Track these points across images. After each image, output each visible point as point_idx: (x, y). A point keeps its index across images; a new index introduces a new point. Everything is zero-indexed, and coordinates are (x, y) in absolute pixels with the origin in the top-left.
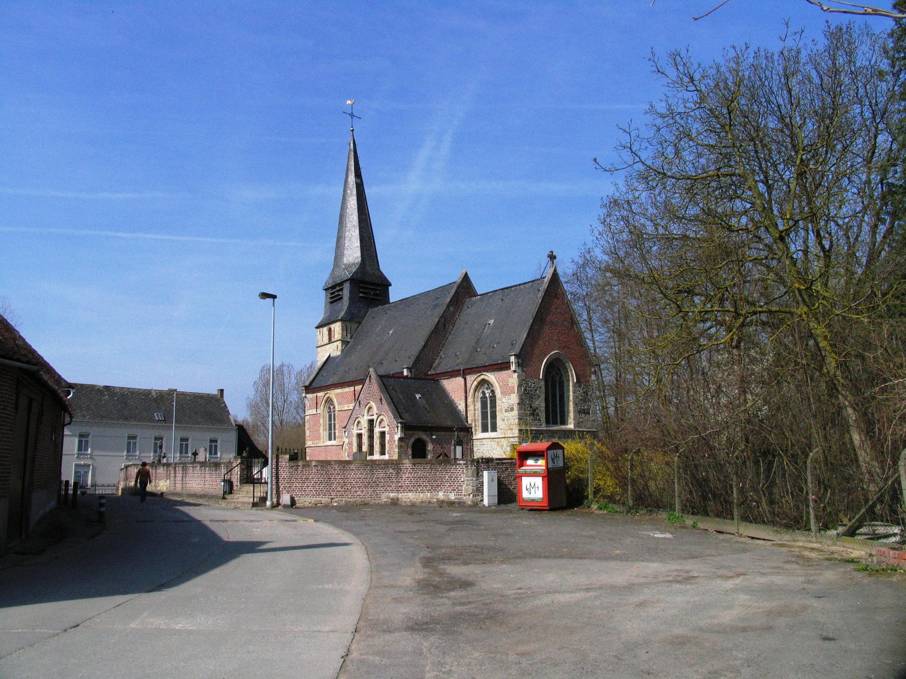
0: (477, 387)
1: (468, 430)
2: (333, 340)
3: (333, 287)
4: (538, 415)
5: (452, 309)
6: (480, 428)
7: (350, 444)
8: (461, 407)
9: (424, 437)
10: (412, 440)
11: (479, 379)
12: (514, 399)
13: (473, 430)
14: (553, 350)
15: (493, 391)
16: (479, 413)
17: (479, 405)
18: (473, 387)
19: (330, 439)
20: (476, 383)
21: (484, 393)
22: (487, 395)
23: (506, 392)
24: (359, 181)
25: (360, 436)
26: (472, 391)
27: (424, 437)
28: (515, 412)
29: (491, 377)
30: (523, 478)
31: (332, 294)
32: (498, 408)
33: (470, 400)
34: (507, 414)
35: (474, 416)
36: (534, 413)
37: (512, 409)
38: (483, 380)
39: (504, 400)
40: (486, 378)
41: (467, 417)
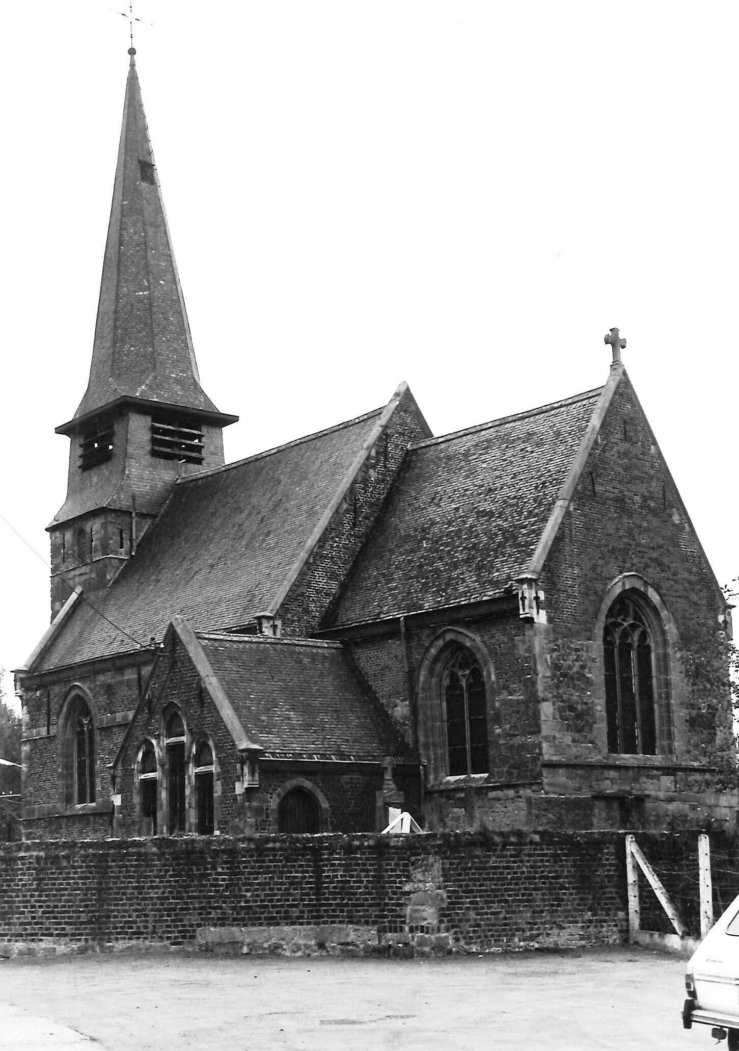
15: (476, 673)
21: (454, 677)
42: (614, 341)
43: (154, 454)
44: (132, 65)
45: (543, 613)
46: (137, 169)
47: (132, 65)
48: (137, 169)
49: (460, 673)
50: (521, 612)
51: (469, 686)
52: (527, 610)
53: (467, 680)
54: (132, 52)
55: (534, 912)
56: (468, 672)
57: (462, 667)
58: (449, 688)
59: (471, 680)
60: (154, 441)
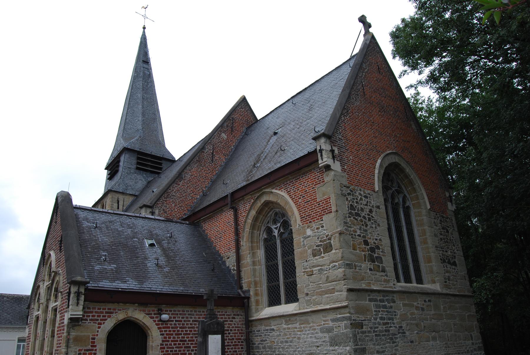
0: (256, 219)
1: (242, 303)
4: (379, 259)
5: (224, 136)
6: (265, 298)
8: (231, 263)
9: (140, 316)
10: (109, 324)
11: (259, 204)
12: (331, 225)
13: (253, 299)
14: (374, 165)
15: (286, 225)
16: (262, 269)
17: (261, 253)
18: (249, 221)
19: (274, 301)
20: (253, 213)
21: (269, 231)
22: (276, 233)
23: (313, 213)
24: (286, 235)
26: (247, 229)
27: (140, 316)
29: (281, 195)
30: (210, 336)
32: (297, 251)
33: (245, 243)
34: (318, 260)
35: (253, 272)
36: (373, 255)
37: (328, 248)
38: (267, 204)
39: (309, 232)
40: (271, 198)
41: (240, 278)
42: (362, 19)
43: (138, 168)
44: (144, 32)
45: (338, 164)
46: (143, 59)
47: (144, 32)
48: (143, 59)
49: (273, 227)
50: (320, 161)
51: (281, 234)
52: (325, 160)
53: (279, 230)
54: (144, 28)
55: (389, 331)
56: (279, 225)
57: (275, 222)
58: (266, 240)
59: (282, 230)
60: (138, 163)
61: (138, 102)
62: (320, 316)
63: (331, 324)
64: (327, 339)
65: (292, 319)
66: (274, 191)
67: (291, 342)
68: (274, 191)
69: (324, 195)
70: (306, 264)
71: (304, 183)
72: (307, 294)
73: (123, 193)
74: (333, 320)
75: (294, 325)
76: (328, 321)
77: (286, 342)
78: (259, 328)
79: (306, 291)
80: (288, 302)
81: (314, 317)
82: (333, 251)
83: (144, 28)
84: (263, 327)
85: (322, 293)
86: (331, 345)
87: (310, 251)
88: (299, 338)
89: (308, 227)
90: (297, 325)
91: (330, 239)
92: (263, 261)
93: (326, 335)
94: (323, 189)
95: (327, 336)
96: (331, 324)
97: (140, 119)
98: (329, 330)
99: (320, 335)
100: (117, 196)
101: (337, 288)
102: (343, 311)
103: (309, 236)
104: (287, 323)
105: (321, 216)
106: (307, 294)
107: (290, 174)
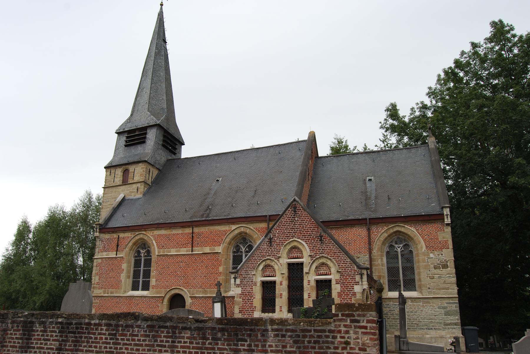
2: (130, 181)
3: (129, 132)
7: (247, 296)
19: (135, 288)
20: (386, 235)
25: (269, 288)
28: (451, 269)
29: (410, 230)
31: (127, 137)
34: (437, 271)
37: (445, 266)
39: (431, 255)
44: (161, 9)
47: (161, 9)
50: (446, 220)
54: (162, 5)
56: (401, 245)
61: (160, 80)
62: (439, 300)
63: (446, 305)
64: (443, 312)
65: (416, 300)
66: (406, 226)
67: (415, 312)
68: (406, 226)
69: (444, 238)
70: (429, 272)
71: (431, 228)
72: (429, 288)
73: (153, 166)
74: (447, 303)
75: (418, 304)
76: (444, 303)
77: (412, 312)
78: (388, 303)
79: (428, 286)
80: (143, 290)
81: (434, 300)
82: (449, 269)
83: (162, 5)
84: (391, 303)
85: (440, 289)
86: (445, 315)
87: (432, 266)
88: (422, 311)
89: (431, 253)
90: (421, 304)
91: (447, 262)
92: (386, 264)
93: (442, 310)
94: (443, 234)
95: (443, 311)
96: (446, 305)
97: (165, 98)
98: (444, 308)
99: (439, 310)
100: (150, 167)
101: (451, 287)
102: (454, 299)
103: (432, 258)
104: (412, 302)
105: (441, 249)
106: (429, 288)
107: (421, 221)
